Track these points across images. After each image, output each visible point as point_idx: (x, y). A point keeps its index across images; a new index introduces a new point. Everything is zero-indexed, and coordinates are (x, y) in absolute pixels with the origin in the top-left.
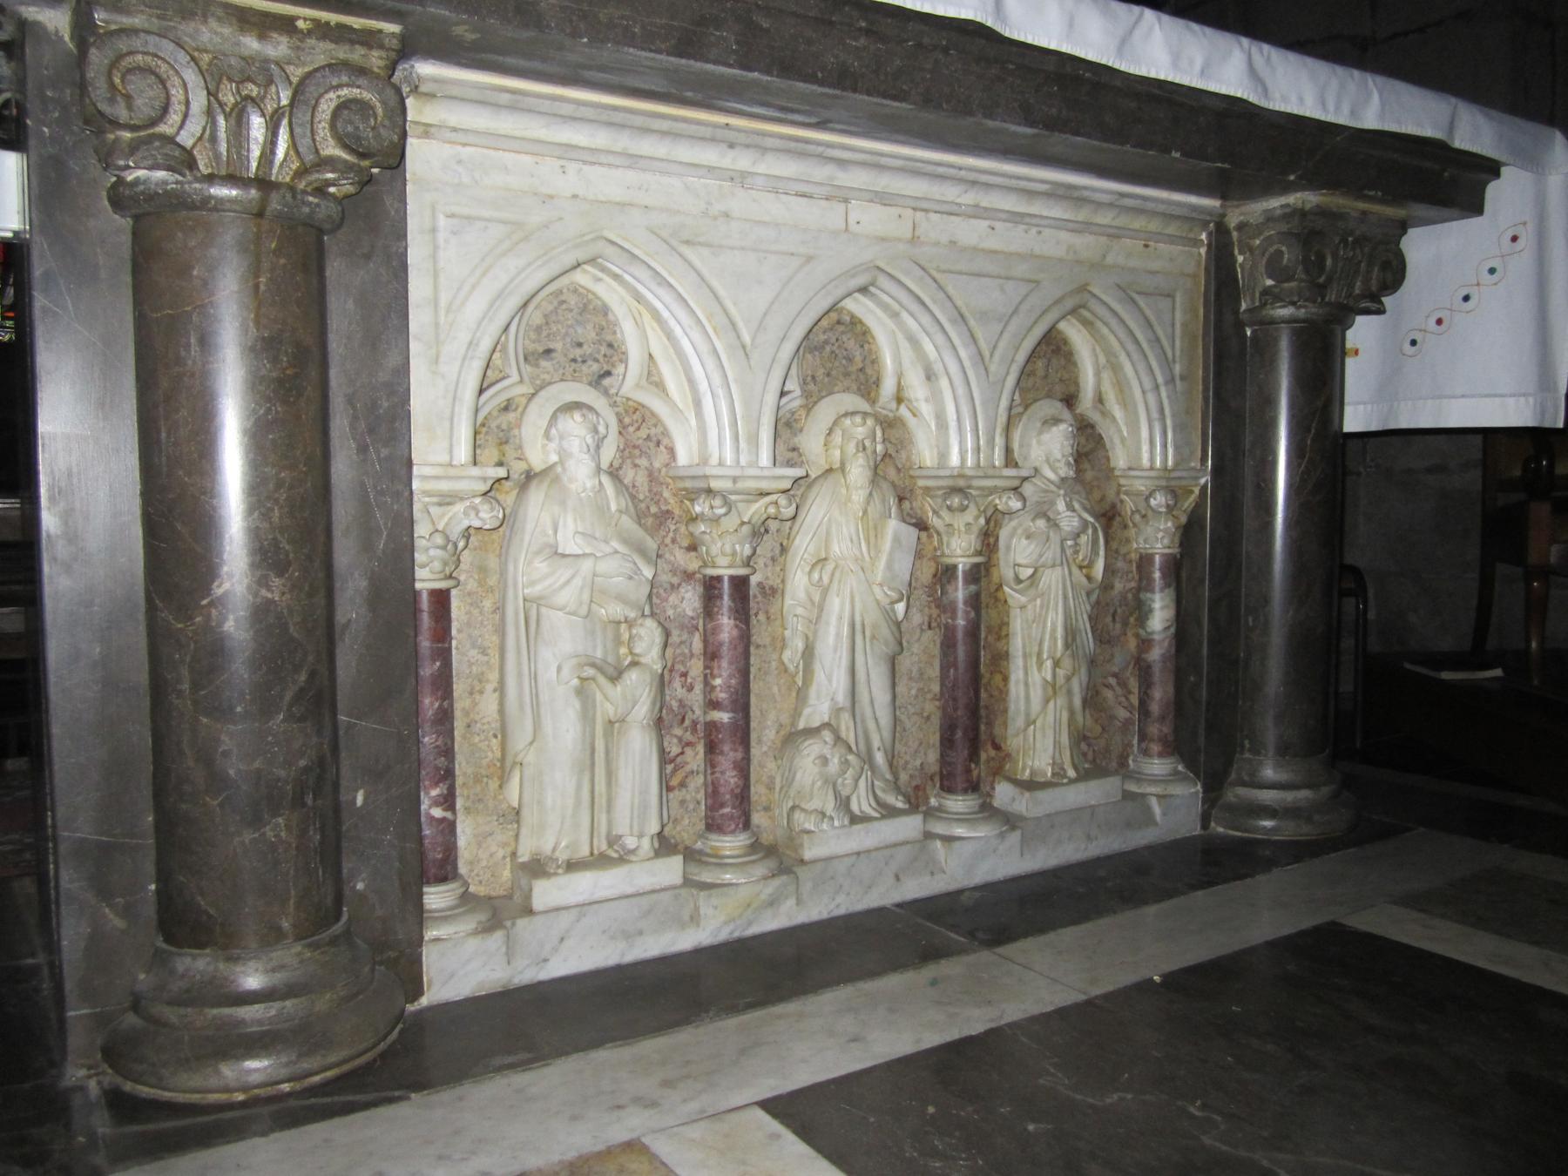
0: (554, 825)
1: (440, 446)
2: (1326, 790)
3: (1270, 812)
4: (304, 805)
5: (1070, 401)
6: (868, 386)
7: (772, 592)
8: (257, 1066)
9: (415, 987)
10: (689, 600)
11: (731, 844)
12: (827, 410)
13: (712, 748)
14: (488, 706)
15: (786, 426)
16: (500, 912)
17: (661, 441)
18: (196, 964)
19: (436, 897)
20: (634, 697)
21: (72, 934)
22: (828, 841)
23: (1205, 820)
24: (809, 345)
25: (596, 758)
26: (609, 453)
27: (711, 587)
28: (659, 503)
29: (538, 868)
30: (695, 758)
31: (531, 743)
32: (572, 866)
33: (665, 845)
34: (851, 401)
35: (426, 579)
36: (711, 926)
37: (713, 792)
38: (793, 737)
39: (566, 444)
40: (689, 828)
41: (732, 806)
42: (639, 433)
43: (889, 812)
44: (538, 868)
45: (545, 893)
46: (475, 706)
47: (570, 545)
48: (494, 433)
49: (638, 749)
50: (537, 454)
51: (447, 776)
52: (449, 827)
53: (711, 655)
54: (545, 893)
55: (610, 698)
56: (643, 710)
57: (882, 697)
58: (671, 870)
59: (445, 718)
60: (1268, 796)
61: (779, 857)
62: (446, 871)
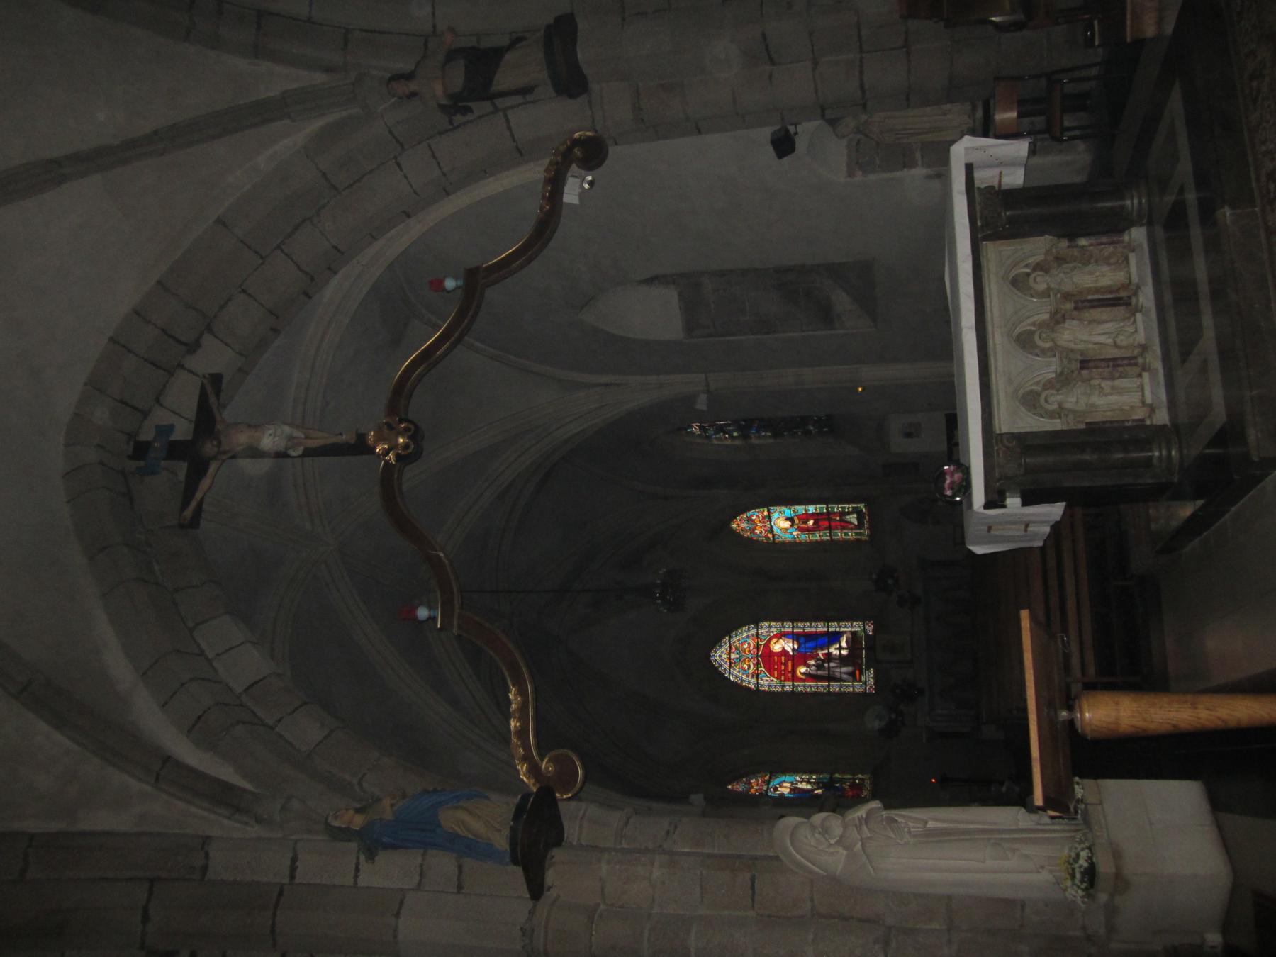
0: (1134, 399)
1: (1057, 425)
2: (1135, 193)
3: (1140, 202)
4: (805, 523)
5: (1028, 275)
6: (1031, 333)
7: (1082, 353)
8: (1173, 453)
9: (1165, 426)
10: (1085, 372)
11: (1140, 360)
12: (1040, 343)
13: (1119, 366)
14: (1109, 413)
15: (1044, 352)
16: (1152, 409)
17: (1050, 381)
18: (1155, 461)
19: (1148, 422)
20: (1106, 384)
21: (1150, 481)
22: (1141, 338)
23: (1142, 225)
24: (1024, 348)
25: (1120, 391)
26: (1053, 392)
27: (1082, 368)
28: (1063, 381)
29: (1143, 402)
30: (1120, 369)
31: (602, 890)
32: (1143, 395)
33: (1140, 376)
34: (1036, 337)
35: (1083, 426)
36: (1158, 365)
37: (1129, 365)
38: (1116, 345)
39: (1054, 400)
40: (1137, 370)
41: (1131, 362)
42: (1049, 385)
43: (1135, 321)
44: (1143, 402)
45: (1149, 400)
46: (1109, 416)
47: (1074, 399)
48: (1051, 415)
49: (1117, 383)
50: (1055, 406)
51: (1123, 421)
52: (1134, 421)
53: (1097, 367)
54: (1149, 400)
55: (1107, 390)
56: (1109, 383)
57: (1109, 325)
58: (1146, 375)
59: (1111, 422)
60: (1136, 201)
61: (1144, 348)
62: (1143, 420)
